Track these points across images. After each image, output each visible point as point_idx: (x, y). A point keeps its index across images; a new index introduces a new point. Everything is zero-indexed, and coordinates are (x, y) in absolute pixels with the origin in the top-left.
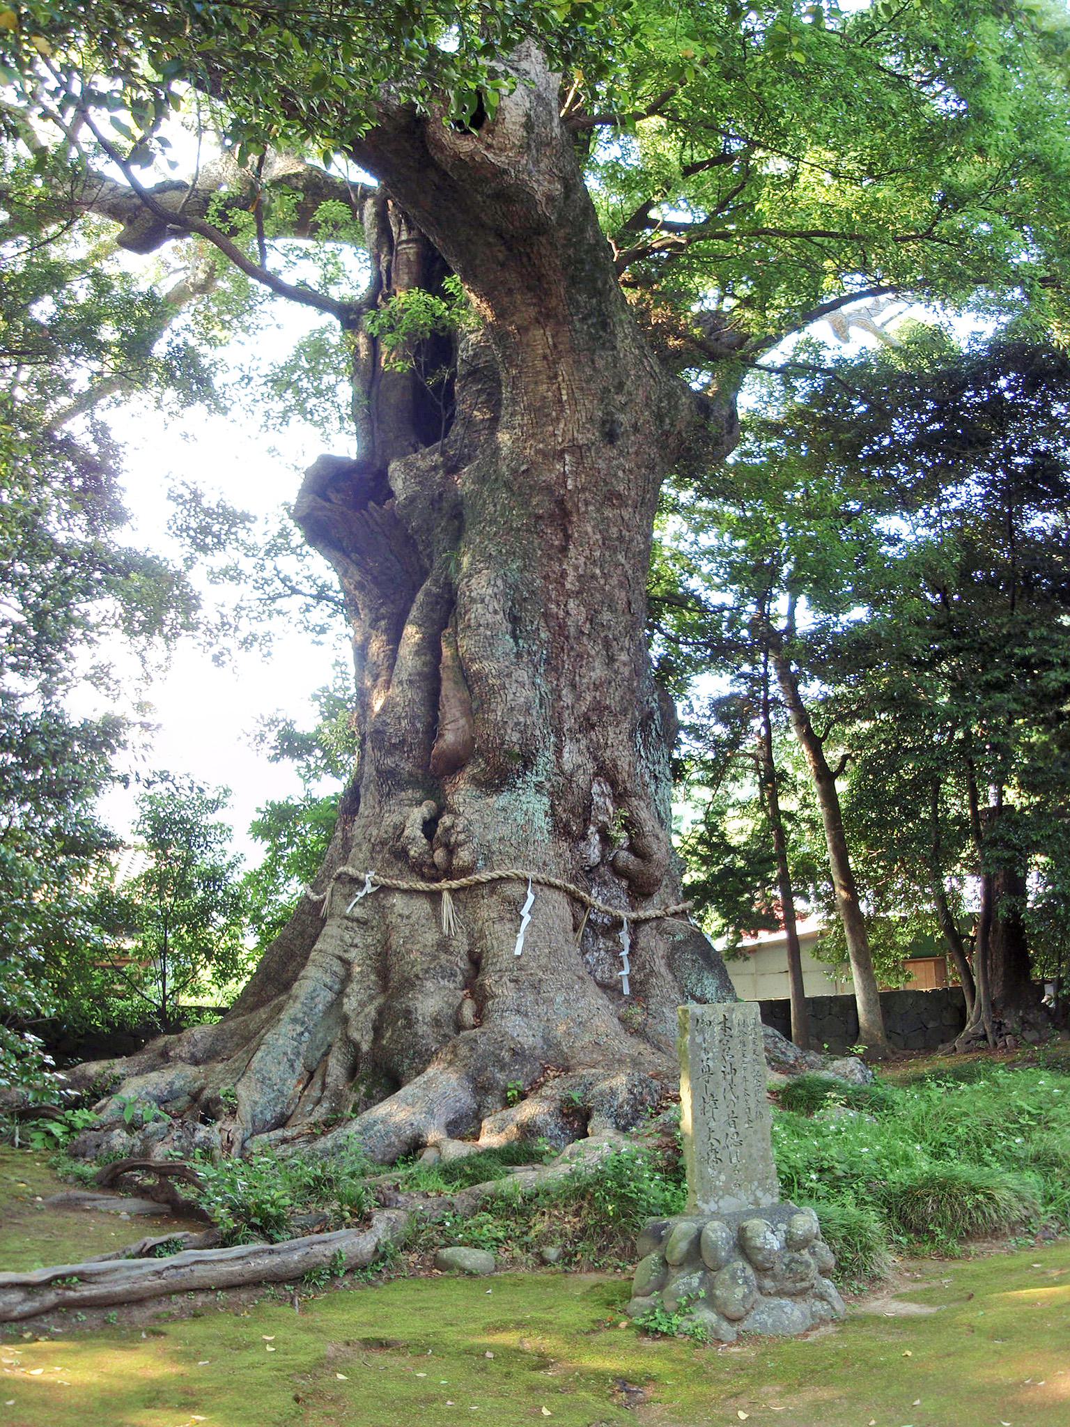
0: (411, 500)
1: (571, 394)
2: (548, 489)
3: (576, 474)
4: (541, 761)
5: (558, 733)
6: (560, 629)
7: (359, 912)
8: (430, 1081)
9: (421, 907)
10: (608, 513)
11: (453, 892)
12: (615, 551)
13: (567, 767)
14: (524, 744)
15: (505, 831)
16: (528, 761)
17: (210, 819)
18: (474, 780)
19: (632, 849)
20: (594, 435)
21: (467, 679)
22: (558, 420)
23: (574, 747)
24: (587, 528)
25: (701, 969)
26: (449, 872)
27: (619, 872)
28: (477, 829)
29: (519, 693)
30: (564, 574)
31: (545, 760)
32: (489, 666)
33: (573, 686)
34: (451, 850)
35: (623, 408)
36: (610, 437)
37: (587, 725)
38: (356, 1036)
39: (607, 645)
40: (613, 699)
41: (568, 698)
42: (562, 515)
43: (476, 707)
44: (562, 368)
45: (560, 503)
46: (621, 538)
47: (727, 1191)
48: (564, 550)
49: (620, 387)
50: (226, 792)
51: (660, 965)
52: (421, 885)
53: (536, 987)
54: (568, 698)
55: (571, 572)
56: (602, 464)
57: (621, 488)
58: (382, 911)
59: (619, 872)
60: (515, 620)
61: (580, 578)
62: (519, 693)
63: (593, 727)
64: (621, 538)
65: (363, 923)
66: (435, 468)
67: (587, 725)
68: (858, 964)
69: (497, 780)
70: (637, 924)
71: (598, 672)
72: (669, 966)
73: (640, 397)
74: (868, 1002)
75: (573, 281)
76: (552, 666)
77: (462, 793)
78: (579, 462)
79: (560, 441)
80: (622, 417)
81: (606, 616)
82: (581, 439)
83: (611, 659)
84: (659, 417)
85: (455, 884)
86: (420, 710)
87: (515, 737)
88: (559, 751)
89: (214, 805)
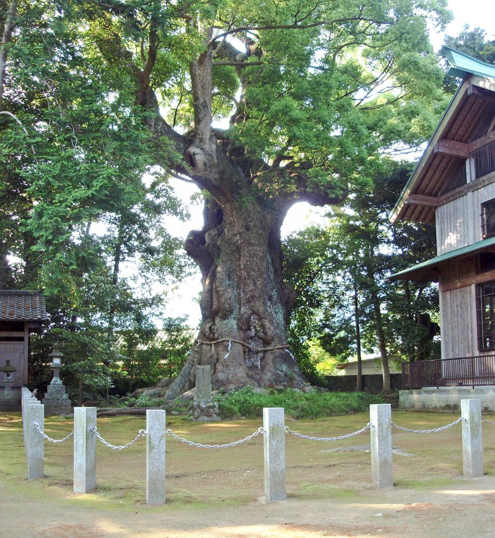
0: (209, 245)
1: (237, 220)
2: (235, 244)
3: (240, 239)
4: (235, 312)
5: (240, 304)
6: (240, 278)
7: (197, 349)
8: (468, 432)
9: (209, 347)
10: (250, 248)
11: (215, 344)
12: (253, 257)
13: (242, 313)
14: (230, 308)
15: (226, 329)
16: (231, 312)
17: (183, 324)
18: (220, 317)
19: (263, 332)
20: (244, 229)
21: (217, 292)
22: (235, 226)
23: (244, 308)
24: (245, 252)
25: (282, 363)
26: (214, 340)
27: (260, 338)
28: (220, 329)
29: (229, 294)
30: (240, 265)
31: (236, 312)
32: (221, 289)
33: (244, 291)
34: (214, 334)
35: (250, 222)
36: (248, 229)
37: (249, 301)
38: (191, 378)
39: (253, 280)
40: (256, 294)
41: (242, 295)
42: (238, 250)
43: (219, 297)
44: (234, 213)
45: (237, 247)
46: (254, 254)
47: (202, 398)
48: (240, 258)
49: (249, 216)
50: (187, 316)
51: (270, 362)
52: (208, 343)
53: (227, 366)
54: (242, 295)
55: (242, 264)
56: (247, 237)
57: (252, 242)
58: (201, 348)
59: (260, 338)
60: (229, 276)
61: (244, 265)
62: (229, 294)
63: (251, 302)
64: (254, 254)
65: (197, 352)
66: (215, 235)
67: (249, 301)
68: (384, 365)
69: (225, 317)
70: (265, 351)
71: (252, 287)
72: (273, 362)
73: (255, 217)
74: (386, 376)
75: (232, 192)
76: (238, 287)
77: (217, 320)
78: (241, 236)
79: (235, 232)
80: (250, 224)
81: (252, 273)
82: (241, 231)
83: (255, 284)
84: (261, 222)
85: (214, 342)
86: (209, 299)
87: (228, 306)
88: (240, 309)
89: (184, 320)
